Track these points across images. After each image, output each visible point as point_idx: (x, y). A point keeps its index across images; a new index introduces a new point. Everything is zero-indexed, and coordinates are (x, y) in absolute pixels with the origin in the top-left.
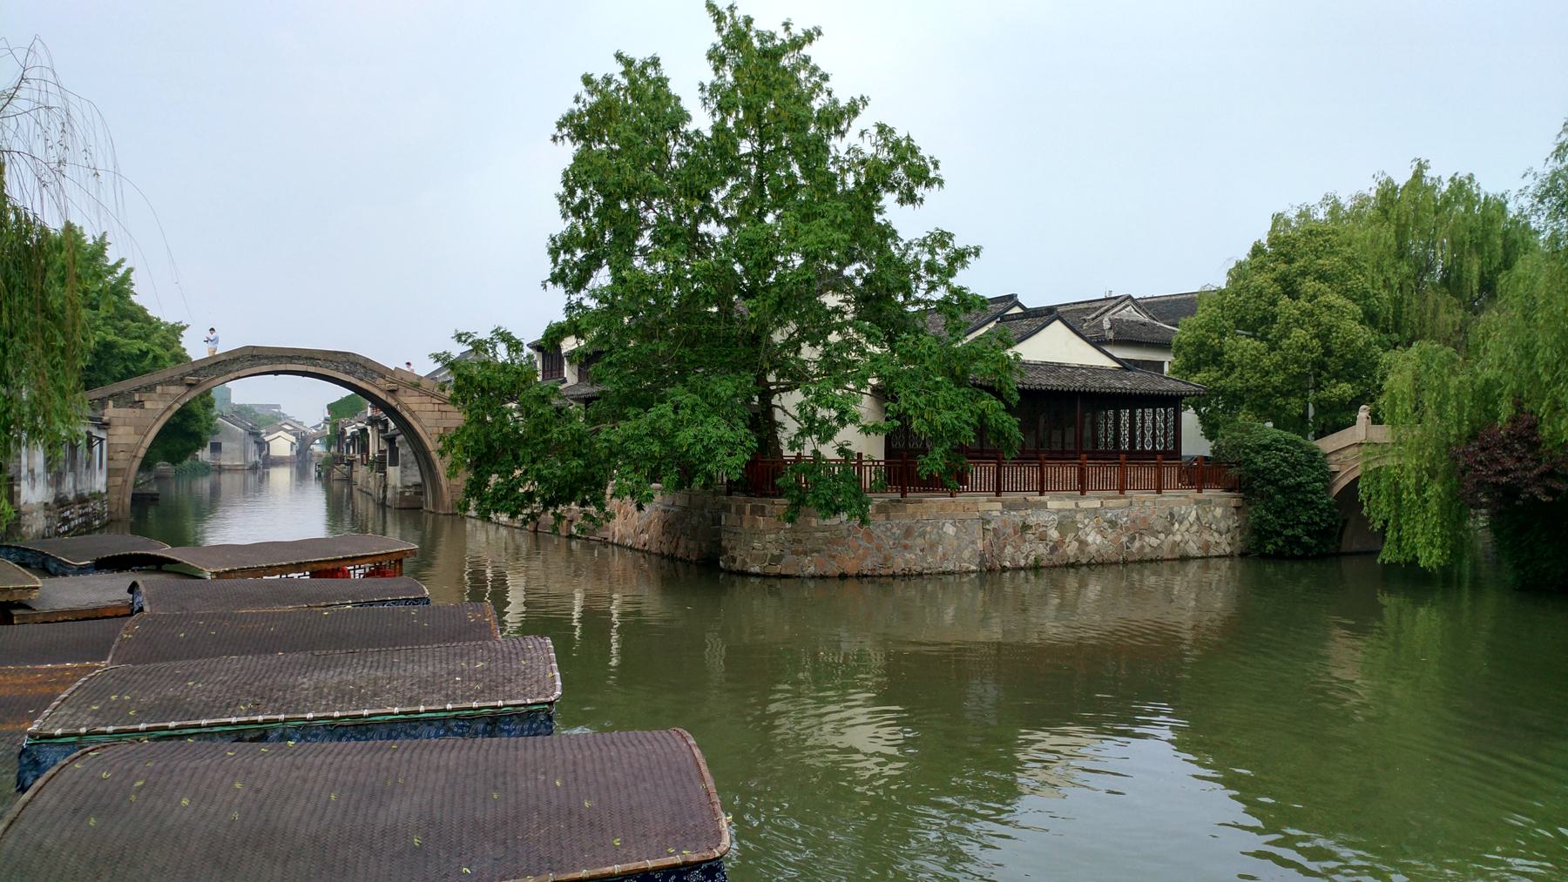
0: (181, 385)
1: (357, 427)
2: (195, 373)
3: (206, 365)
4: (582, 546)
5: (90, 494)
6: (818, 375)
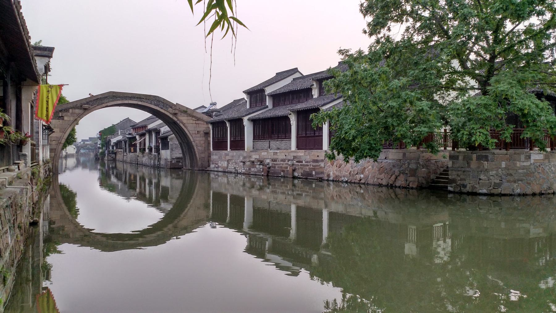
0: (81, 109)
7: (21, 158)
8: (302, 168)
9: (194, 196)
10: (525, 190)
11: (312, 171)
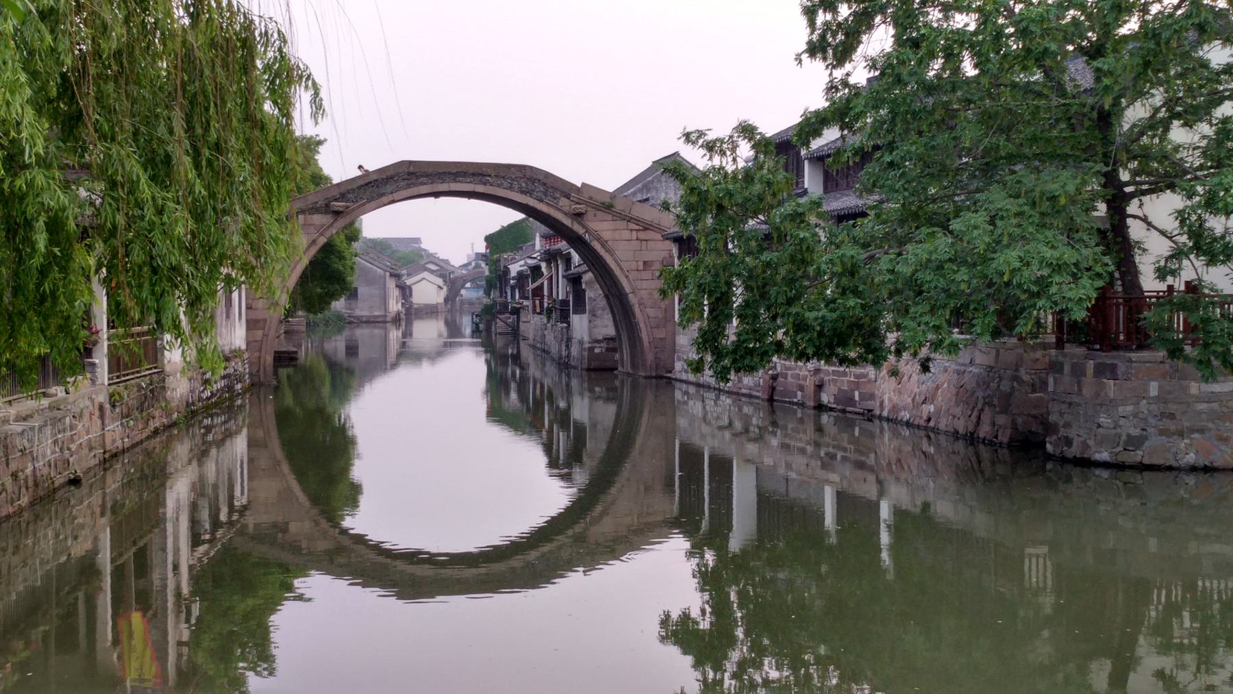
0: (326, 213)
1: (526, 264)
2: (343, 197)
3: (355, 186)
4: (837, 419)
5: (231, 352)
6: (1201, 167)
7: (87, 368)
8: (835, 381)
9: (635, 452)
10: (1211, 457)
11: (853, 391)
